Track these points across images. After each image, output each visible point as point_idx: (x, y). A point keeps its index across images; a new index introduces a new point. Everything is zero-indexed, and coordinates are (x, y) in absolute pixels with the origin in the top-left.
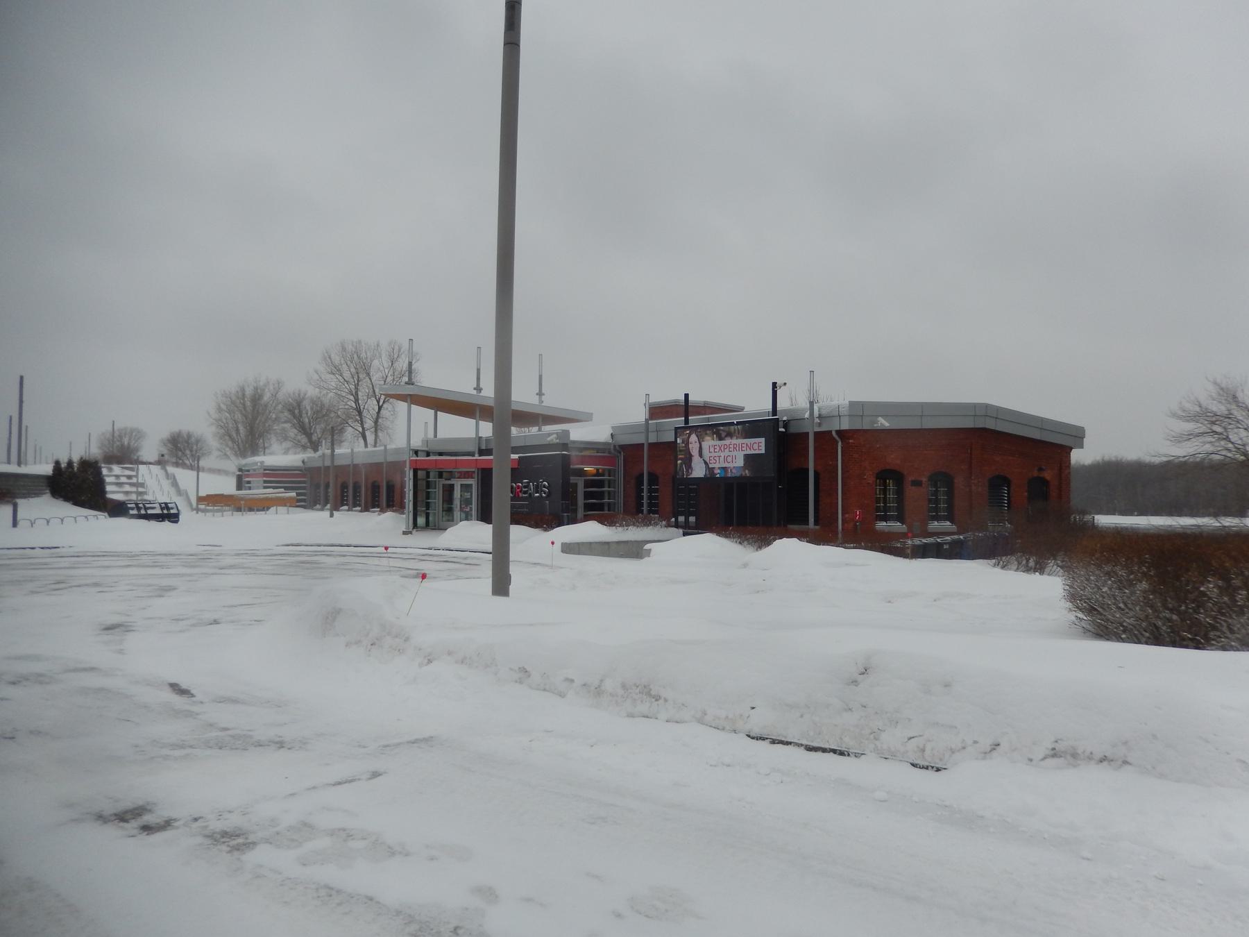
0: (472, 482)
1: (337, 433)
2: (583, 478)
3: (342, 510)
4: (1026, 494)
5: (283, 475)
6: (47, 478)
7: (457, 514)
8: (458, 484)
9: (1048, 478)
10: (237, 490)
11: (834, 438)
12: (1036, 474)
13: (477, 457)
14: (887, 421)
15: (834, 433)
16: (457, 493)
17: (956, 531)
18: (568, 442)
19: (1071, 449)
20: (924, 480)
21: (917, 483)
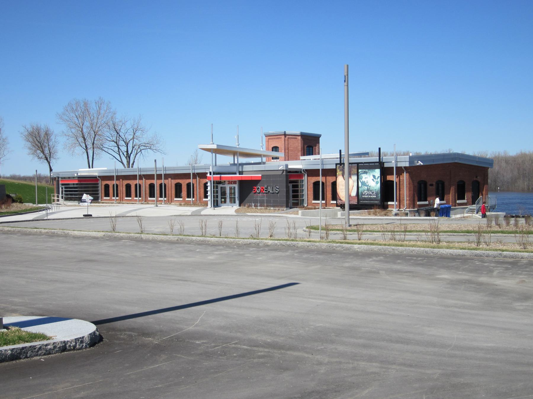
0: (236, 186)
1: (426, 234)
2: (292, 184)
3: (172, 204)
4: (471, 187)
5: (85, 181)
6: (201, 212)
7: (228, 200)
8: (228, 187)
9: (479, 181)
10: (302, 216)
11: (403, 169)
12: (475, 179)
13: (238, 175)
14: (422, 163)
15: (403, 168)
16: (228, 191)
17: (445, 203)
18: (288, 169)
19: (488, 168)
20: (434, 183)
21: (432, 185)
